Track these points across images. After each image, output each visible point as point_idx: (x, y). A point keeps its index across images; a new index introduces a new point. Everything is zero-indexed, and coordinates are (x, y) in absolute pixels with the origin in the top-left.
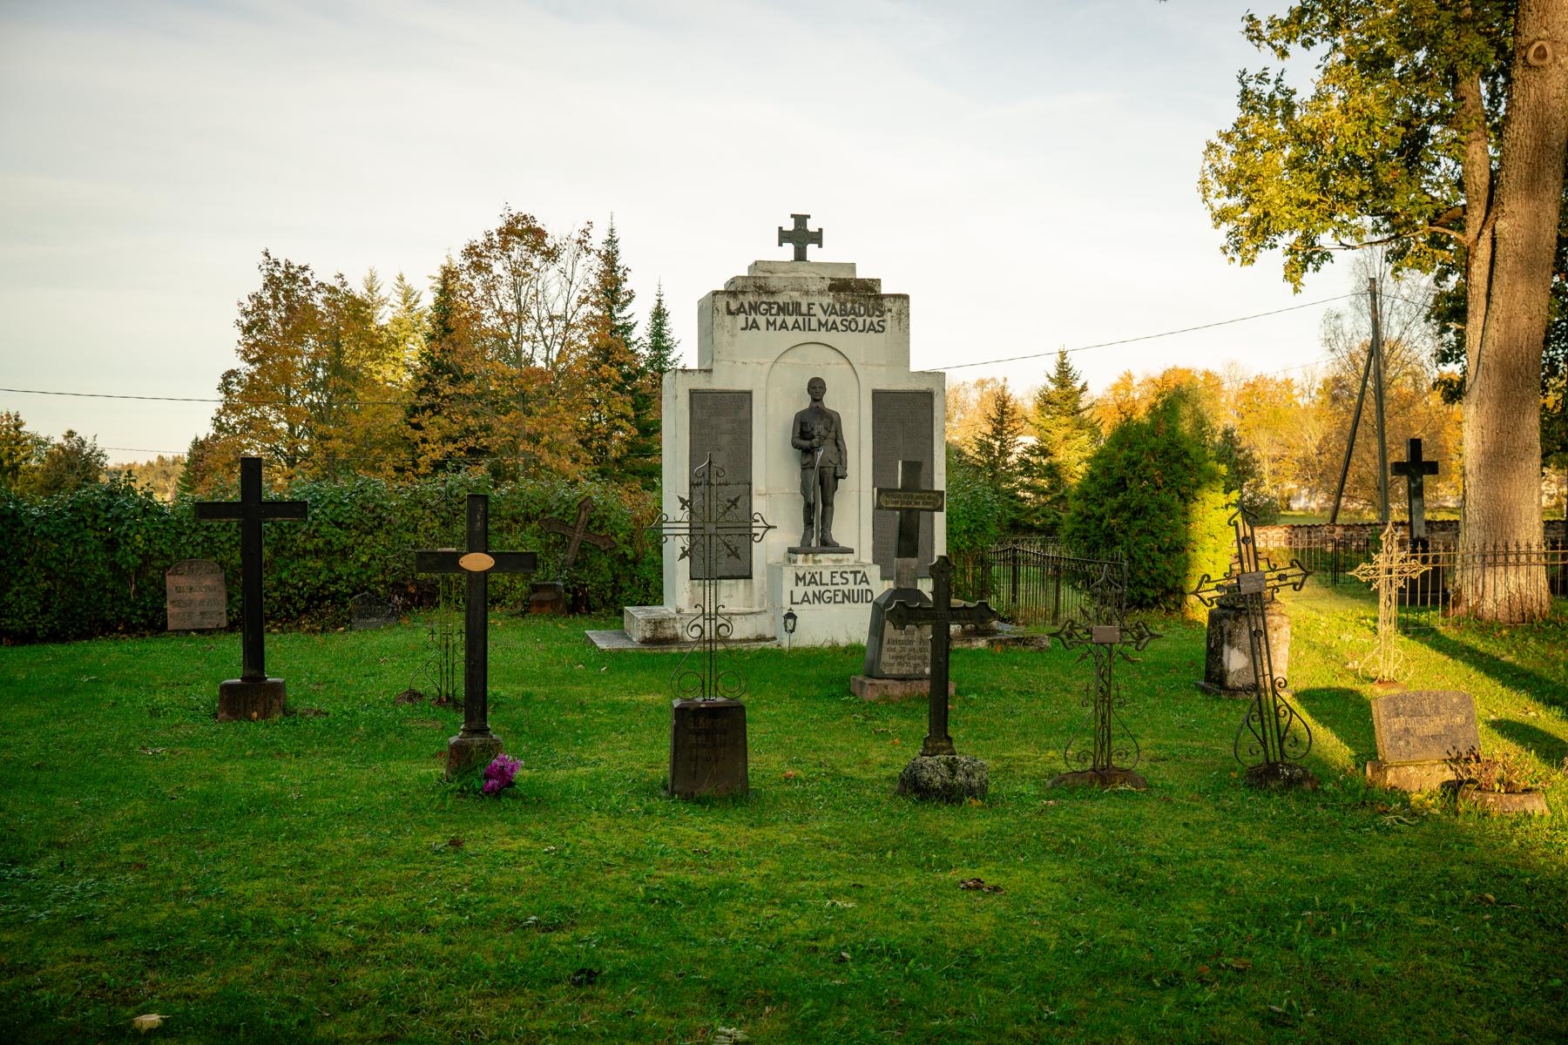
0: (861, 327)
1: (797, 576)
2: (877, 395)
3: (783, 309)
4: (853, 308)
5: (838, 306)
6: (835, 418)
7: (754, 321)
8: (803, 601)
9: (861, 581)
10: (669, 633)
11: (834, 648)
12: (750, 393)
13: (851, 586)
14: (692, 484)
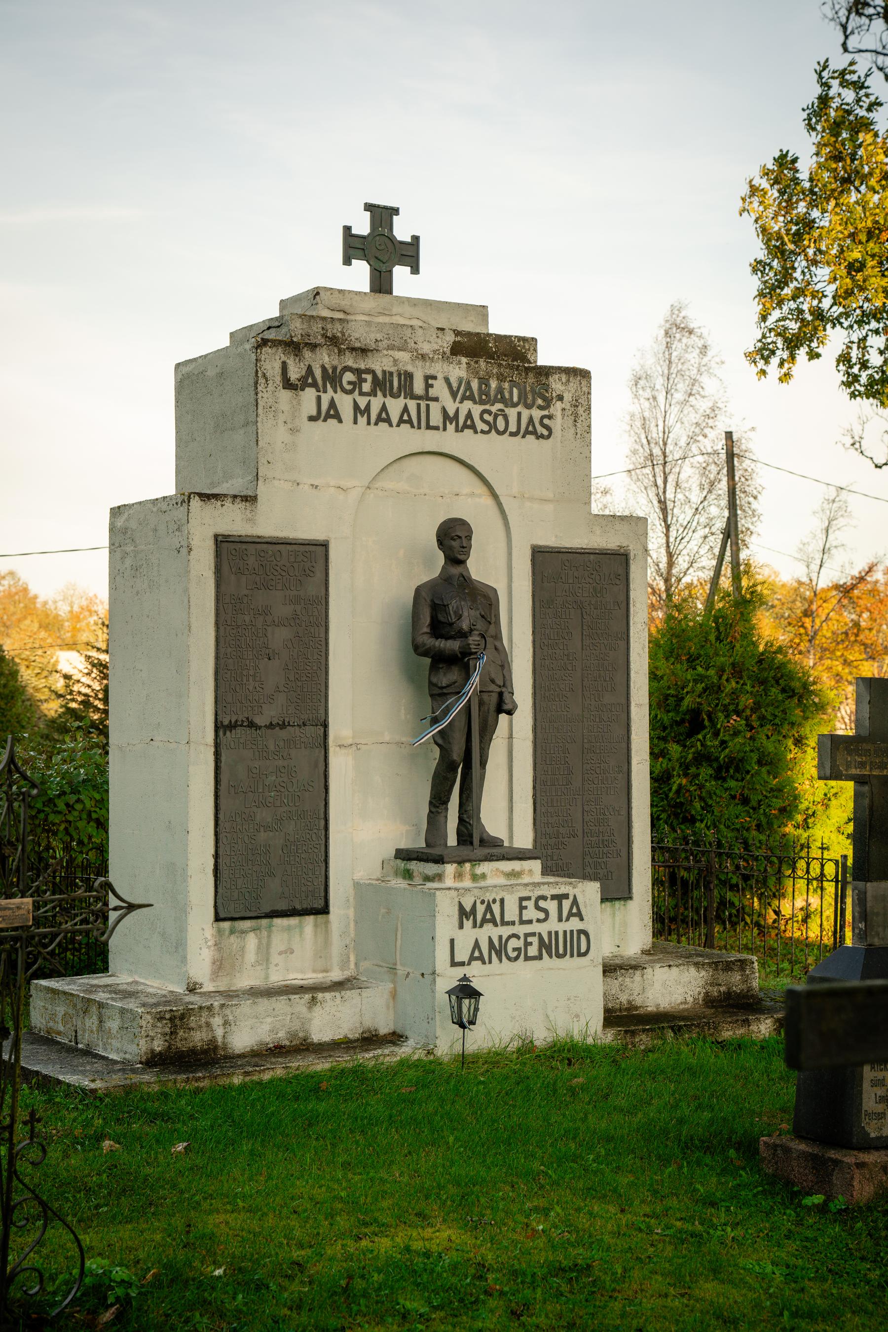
0: (513, 428)
1: (461, 907)
2: (539, 554)
3: (382, 384)
4: (500, 390)
5: (475, 385)
6: (491, 595)
7: (332, 404)
8: (472, 958)
9: (571, 915)
10: (198, 1038)
11: (527, 1049)
12: (324, 545)
13: (553, 925)
14: (217, 728)
